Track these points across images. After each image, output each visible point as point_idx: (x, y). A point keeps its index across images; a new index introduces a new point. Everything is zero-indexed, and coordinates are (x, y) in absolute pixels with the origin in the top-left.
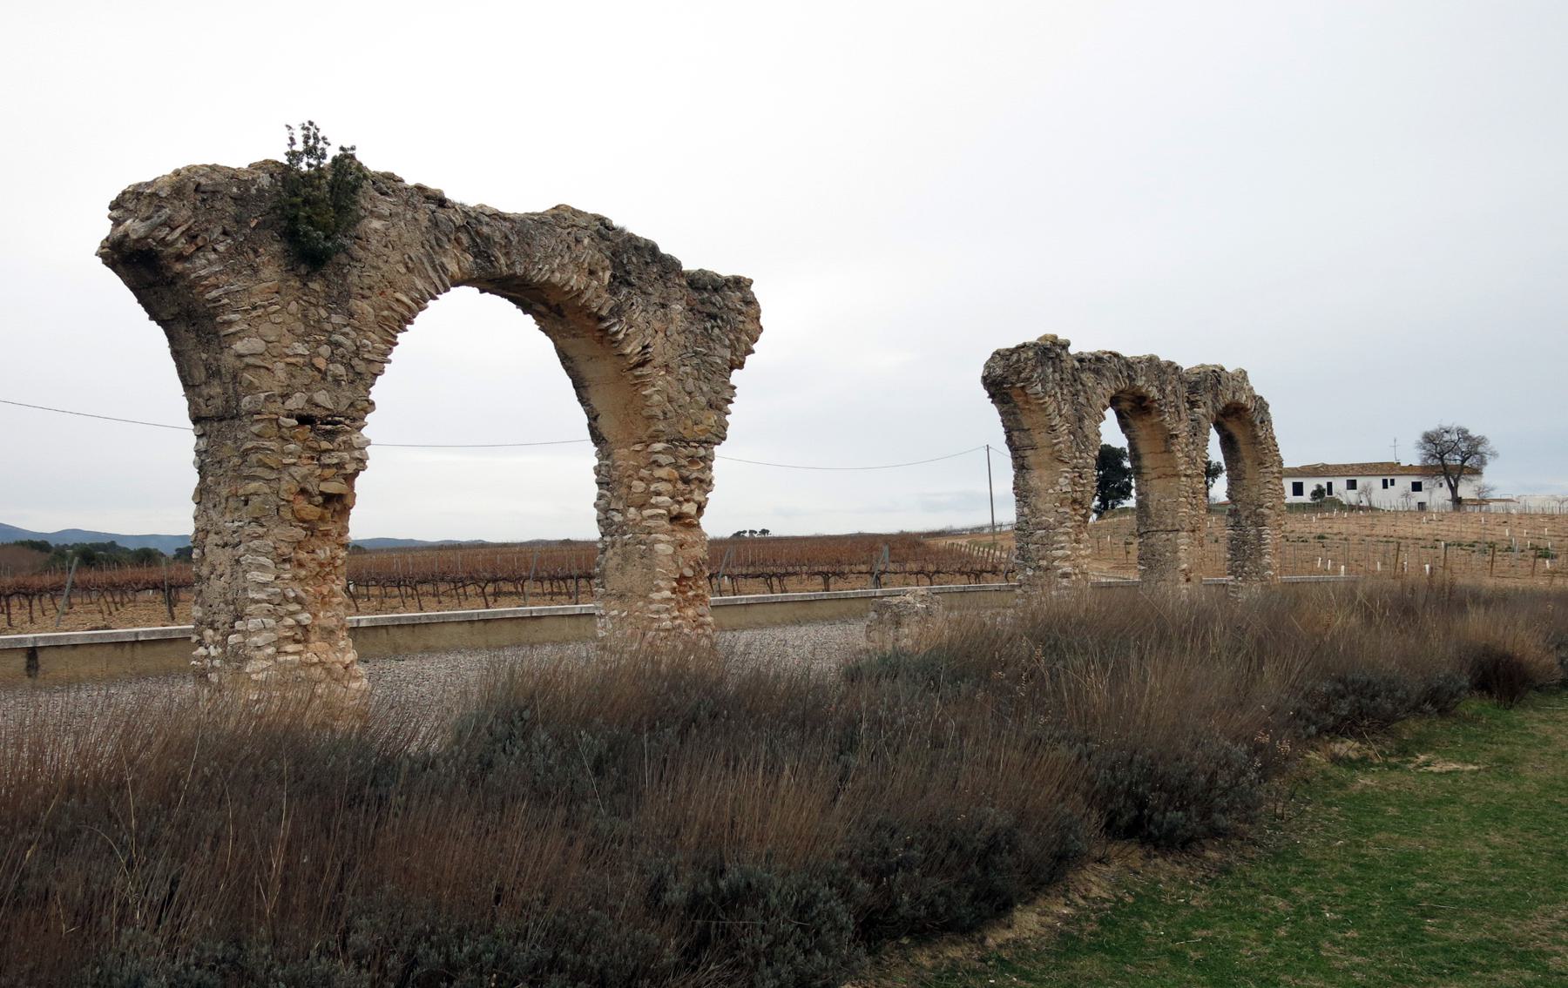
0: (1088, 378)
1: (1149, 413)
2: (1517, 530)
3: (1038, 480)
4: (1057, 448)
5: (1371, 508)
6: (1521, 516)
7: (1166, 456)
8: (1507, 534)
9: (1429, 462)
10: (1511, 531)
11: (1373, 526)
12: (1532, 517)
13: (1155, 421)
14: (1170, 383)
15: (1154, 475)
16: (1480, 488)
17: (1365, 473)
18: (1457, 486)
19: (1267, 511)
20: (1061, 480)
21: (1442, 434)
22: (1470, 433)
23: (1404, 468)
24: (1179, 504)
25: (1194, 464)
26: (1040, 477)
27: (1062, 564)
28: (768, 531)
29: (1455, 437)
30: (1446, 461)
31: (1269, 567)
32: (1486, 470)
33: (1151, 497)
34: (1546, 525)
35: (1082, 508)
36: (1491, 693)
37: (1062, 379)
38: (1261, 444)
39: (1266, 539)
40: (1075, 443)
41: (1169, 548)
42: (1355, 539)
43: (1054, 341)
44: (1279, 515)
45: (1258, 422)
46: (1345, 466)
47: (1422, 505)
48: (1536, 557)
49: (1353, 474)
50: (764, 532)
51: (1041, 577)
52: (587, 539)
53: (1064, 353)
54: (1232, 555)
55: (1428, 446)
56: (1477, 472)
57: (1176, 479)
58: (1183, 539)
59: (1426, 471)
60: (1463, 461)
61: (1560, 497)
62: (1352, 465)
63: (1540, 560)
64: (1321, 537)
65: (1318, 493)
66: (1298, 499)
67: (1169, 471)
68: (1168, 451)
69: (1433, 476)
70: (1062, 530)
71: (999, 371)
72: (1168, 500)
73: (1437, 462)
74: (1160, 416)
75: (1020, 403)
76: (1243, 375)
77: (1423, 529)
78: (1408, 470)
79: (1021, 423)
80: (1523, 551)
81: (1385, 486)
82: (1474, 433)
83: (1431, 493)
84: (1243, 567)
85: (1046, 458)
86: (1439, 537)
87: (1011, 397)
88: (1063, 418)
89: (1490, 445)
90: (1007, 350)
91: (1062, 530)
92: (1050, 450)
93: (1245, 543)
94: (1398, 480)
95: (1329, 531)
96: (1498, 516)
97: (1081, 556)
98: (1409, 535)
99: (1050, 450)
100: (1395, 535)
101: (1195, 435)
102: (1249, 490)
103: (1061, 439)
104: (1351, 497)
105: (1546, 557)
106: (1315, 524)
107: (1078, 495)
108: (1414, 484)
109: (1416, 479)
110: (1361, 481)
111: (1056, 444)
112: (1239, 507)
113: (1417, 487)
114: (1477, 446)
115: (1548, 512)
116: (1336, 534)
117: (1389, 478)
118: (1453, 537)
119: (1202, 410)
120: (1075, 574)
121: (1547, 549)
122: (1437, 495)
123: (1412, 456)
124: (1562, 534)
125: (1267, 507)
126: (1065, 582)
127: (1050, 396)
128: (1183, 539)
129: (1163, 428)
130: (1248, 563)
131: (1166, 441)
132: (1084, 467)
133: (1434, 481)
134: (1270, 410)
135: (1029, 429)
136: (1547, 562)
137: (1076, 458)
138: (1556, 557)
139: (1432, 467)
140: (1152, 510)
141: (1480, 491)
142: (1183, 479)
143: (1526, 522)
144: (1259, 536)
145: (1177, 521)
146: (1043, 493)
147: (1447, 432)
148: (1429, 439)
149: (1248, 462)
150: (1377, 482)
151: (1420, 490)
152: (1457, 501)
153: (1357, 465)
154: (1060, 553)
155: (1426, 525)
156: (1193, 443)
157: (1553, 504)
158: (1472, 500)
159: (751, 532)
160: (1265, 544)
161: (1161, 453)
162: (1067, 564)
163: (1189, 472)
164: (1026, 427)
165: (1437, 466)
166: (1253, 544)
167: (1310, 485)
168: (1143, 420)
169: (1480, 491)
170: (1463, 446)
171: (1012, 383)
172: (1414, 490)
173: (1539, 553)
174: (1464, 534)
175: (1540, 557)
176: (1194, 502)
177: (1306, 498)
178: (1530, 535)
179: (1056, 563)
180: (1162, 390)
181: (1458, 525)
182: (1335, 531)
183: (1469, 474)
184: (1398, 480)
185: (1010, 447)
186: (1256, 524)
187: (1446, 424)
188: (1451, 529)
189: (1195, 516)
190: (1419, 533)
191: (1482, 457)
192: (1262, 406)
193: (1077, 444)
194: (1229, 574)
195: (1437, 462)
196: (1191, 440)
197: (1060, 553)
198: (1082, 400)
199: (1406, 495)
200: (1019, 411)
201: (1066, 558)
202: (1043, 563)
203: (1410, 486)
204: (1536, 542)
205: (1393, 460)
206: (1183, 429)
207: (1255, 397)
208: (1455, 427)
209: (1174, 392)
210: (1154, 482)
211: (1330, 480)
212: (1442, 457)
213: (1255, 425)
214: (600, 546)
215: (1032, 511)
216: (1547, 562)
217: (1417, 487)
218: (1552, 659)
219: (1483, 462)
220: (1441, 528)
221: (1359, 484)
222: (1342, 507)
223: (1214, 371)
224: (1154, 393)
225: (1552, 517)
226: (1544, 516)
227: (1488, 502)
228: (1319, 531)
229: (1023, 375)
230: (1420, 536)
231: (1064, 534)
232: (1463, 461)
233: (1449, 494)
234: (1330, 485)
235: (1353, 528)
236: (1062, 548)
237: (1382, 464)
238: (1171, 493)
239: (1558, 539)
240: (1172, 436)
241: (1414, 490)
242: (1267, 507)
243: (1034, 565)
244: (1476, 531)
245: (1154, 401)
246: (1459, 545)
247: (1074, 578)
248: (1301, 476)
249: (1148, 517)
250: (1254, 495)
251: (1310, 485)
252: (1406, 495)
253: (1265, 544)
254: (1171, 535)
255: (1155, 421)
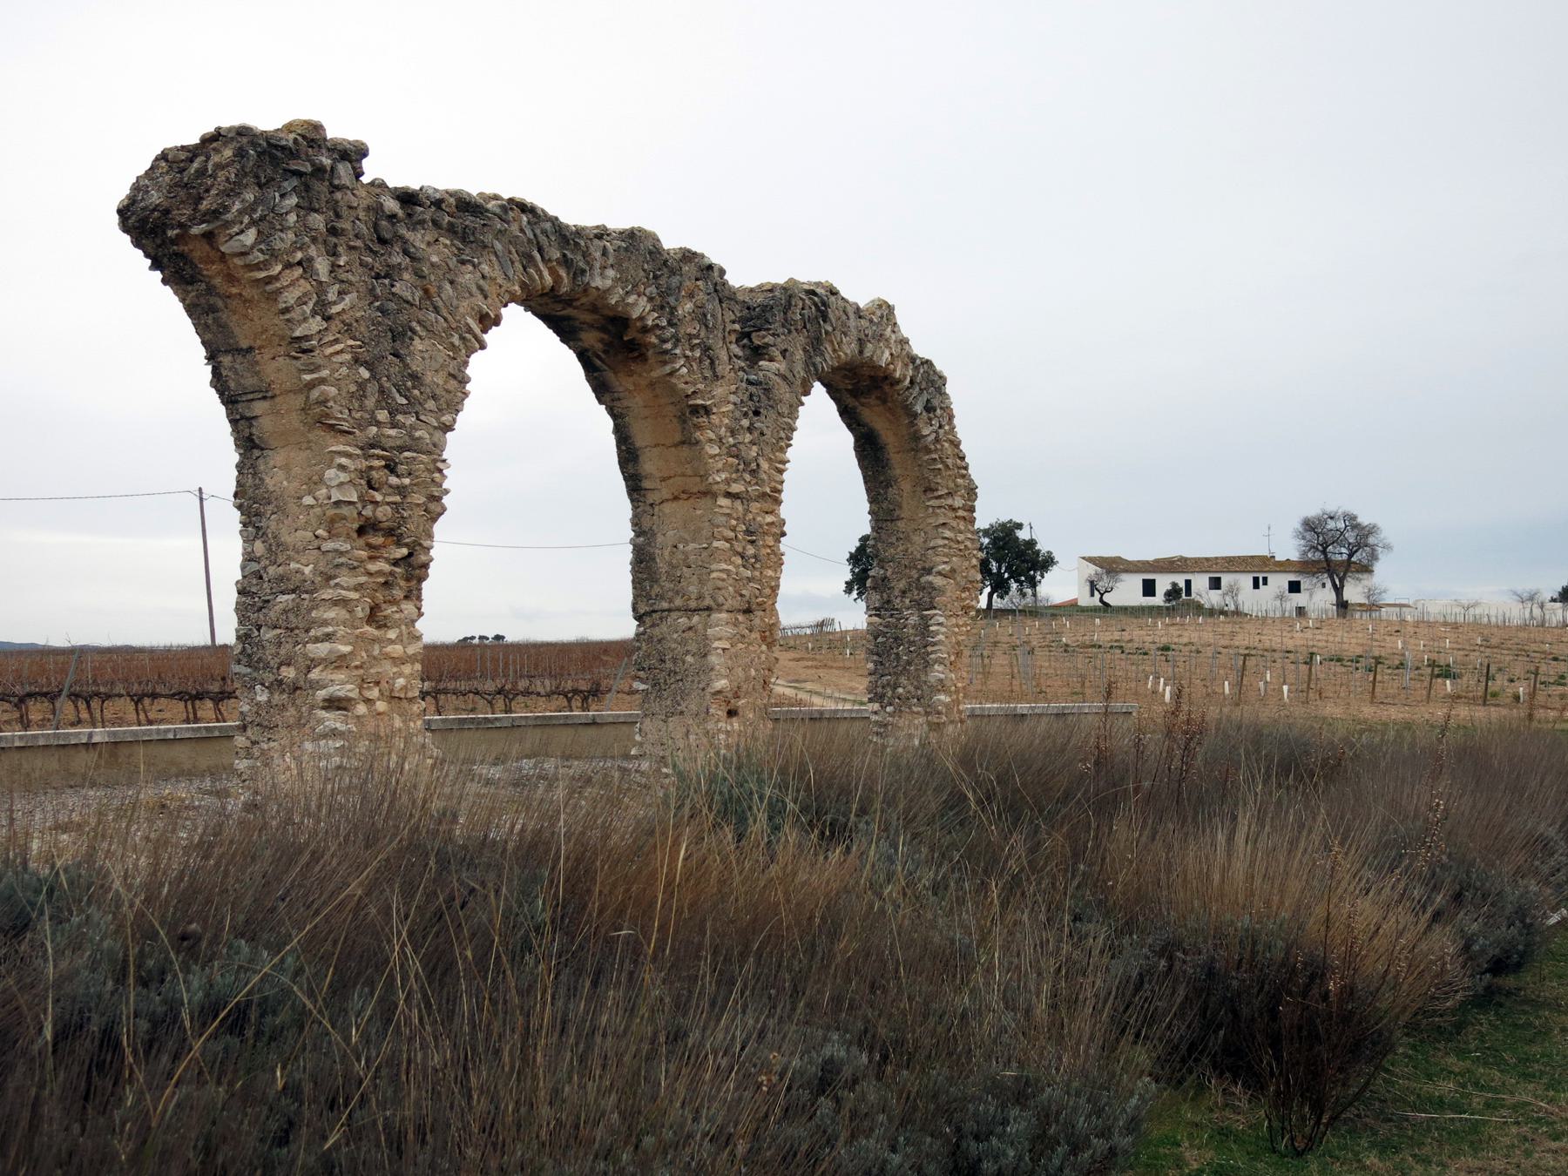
0: (436, 250)
1: (643, 358)
2: (1412, 641)
3: (280, 475)
4: (315, 394)
5: (1237, 613)
6: (1417, 624)
7: (685, 452)
8: (1400, 647)
9: (1310, 555)
10: (1404, 643)
11: (1233, 634)
12: (1430, 625)
13: (655, 374)
14: (691, 296)
15: (666, 494)
16: (1369, 590)
17: (1233, 568)
18: (1342, 586)
19: (938, 581)
20: (331, 473)
21: (1325, 521)
22: (1359, 520)
23: (1280, 564)
24: (713, 554)
25: (753, 472)
26: (286, 468)
27: (328, 675)
28: (503, 637)
29: (1341, 525)
30: (1330, 555)
31: (942, 686)
32: (1378, 567)
33: (660, 538)
34: (1448, 635)
35: (399, 544)
36: (1256, 1084)
37: (333, 231)
38: (929, 451)
39: (937, 633)
40: (372, 388)
41: (693, 647)
42: (1209, 651)
43: (310, 135)
44: (964, 589)
45: (919, 408)
46: (1207, 559)
47: (1301, 611)
48: (1433, 676)
49: (1217, 569)
50: (498, 638)
51: (284, 707)
52: (119, 641)
53: (344, 170)
54: (875, 662)
55: (1308, 535)
56: (1366, 569)
57: (707, 501)
58: (721, 628)
59: (1306, 567)
60: (1351, 555)
61: (1465, 603)
62: (1217, 558)
63: (1439, 680)
64: (1166, 648)
65: (1173, 593)
66: (1150, 601)
67: (694, 485)
68: (688, 442)
69: (1314, 574)
70: (327, 594)
71: (155, 198)
72: (692, 546)
73: (1318, 556)
74: (665, 363)
75: (217, 281)
76: (885, 312)
77: (1297, 639)
78: (1285, 566)
79: (231, 335)
80: (1418, 668)
81: (1256, 585)
82: (1364, 520)
83: (1311, 595)
84: (895, 687)
85: (295, 420)
86: (1315, 650)
87: (194, 266)
88: (336, 325)
89: (1382, 536)
90: (183, 148)
91: (327, 594)
92: (299, 401)
93: (897, 640)
94: (1271, 578)
95: (1176, 640)
96: (1390, 623)
97: (388, 657)
98: (1275, 646)
99: (299, 401)
100: (1260, 646)
101: (757, 413)
102: (908, 539)
103: (325, 373)
104: (1213, 598)
105: (1446, 677)
106: (1161, 631)
107: (384, 513)
108: (1291, 583)
109: (1293, 578)
110: (1226, 579)
111: (311, 386)
112: (889, 573)
113: (1294, 587)
114: (1367, 536)
115: (1450, 619)
116: (1185, 645)
117: (1261, 576)
118: (1333, 649)
119: (779, 365)
120: (368, 701)
121: (1448, 666)
122: (1319, 597)
123: (1289, 548)
124: (1467, 648)
125: (939, 573)
126: (332, 720)
127: (288, 266)
128: (721, 628)
129: (673, 389)
130: (903, 680)
131: (683, 420)
132: (401, 449)
133: (1315, 580)
134: (949, 389)
135: (250, 349)
136: (1448, 682)
137: (378, 424)
138: (1460, 676)
139: (1314, 562)
140: (662, 566)
141: (1370, 593)
142: (723, 501)
143: (1423, 631)
144: (924, 628)
145: (707, 590)
146: (292, 507)
147: (1332, 518)
148: (1311, 526)
149: (906, 486)
150: (1246, 581)
151: (1298, 591)
152: (1342, 605)
153: (1223, 558)
154: (321, 650)
155: (1299, 635)
156: (750, 429)
157: (1457, 610)
158: (1361, 605)
159: (481, 638)
160: (934, 644)
161: (676, 446)
162: (340, 676)
163: (736, 488)
164: (244, 344)
165: (1318, 562)
166: (912, 643)
167: (1163, 583)
168: (631, 374)
169: (1370, 593)
170: (1351, 537)
171: (181, 225)
172: (1291, 591)
173: (1437, 671)
174: (1345, 647)
175: (1438, 676)
176: (751, 551)
177: (1158, 600)
178: (1427, 649)
179: (315, 675)
180: (663, 304)
181: (1339, 634)
182: (1185, 640)
183: (1358, 571)
184: (1271, 578)
185: (221, 394)
186: (919, 605)
187: (1331, 508)
188: (1331, 639)
189: (749, 580)
190: (1290, 645)
191: (1373, 550)
192: (930, 379)
193: (382, 391)
194: (871, 700)
195: (1318, 556)
196: (745, 423)
197: (321, 650)
198: (404, 287)
199: (1281, 597)
200: (220, 304)
201: (340, 662)
202: (289, 673)
203: (1286, 586)
204: (1434, 656)
205: (1266, 553)
206: (724, 396)
207: (913, 359)
208: (1340, 511)
209: (701, 316)
210: (668, 508)
211: (1188, 577)
212: (1325, 549)
213: (915, 415)
214: (923, 678)
215: (269, 550)
216: (1448, 682)
217: (1294, 587)
218: (1444, 943)
219: (1374, 557)
220: (1318, 637)
221: (1224, 583)
222: (1199, 608)
223: (813, 293)
224: (640, 307)
225: (1455, 626)
226: (1445, 624)
227: (1381, 607)
228: (1164, 640)
229: (204, 205)
230: (1290, 648)
231: (336, 603)
232: (1351, 555)
233: (1332, 597)
234: (1188, 583)
235: (1208, 636)
236: (328, 637)
237: (1252, 557)
238: (698, 530)
239: (1462, 653)
240: (695, 410)
241: (1291, 591)
242: (939, 573)
243: (269, 677)
244: (1360, 641)
245: (645, 330)
246: (1339, 660)
247: (361, 709)
248: (1154, 572)
249: (654, 580)
250: (916, 549)
251: (1163, 583)
252: (1281, 597)
253: (934, 644)
254: (696, 619)
255: (655, 374)
